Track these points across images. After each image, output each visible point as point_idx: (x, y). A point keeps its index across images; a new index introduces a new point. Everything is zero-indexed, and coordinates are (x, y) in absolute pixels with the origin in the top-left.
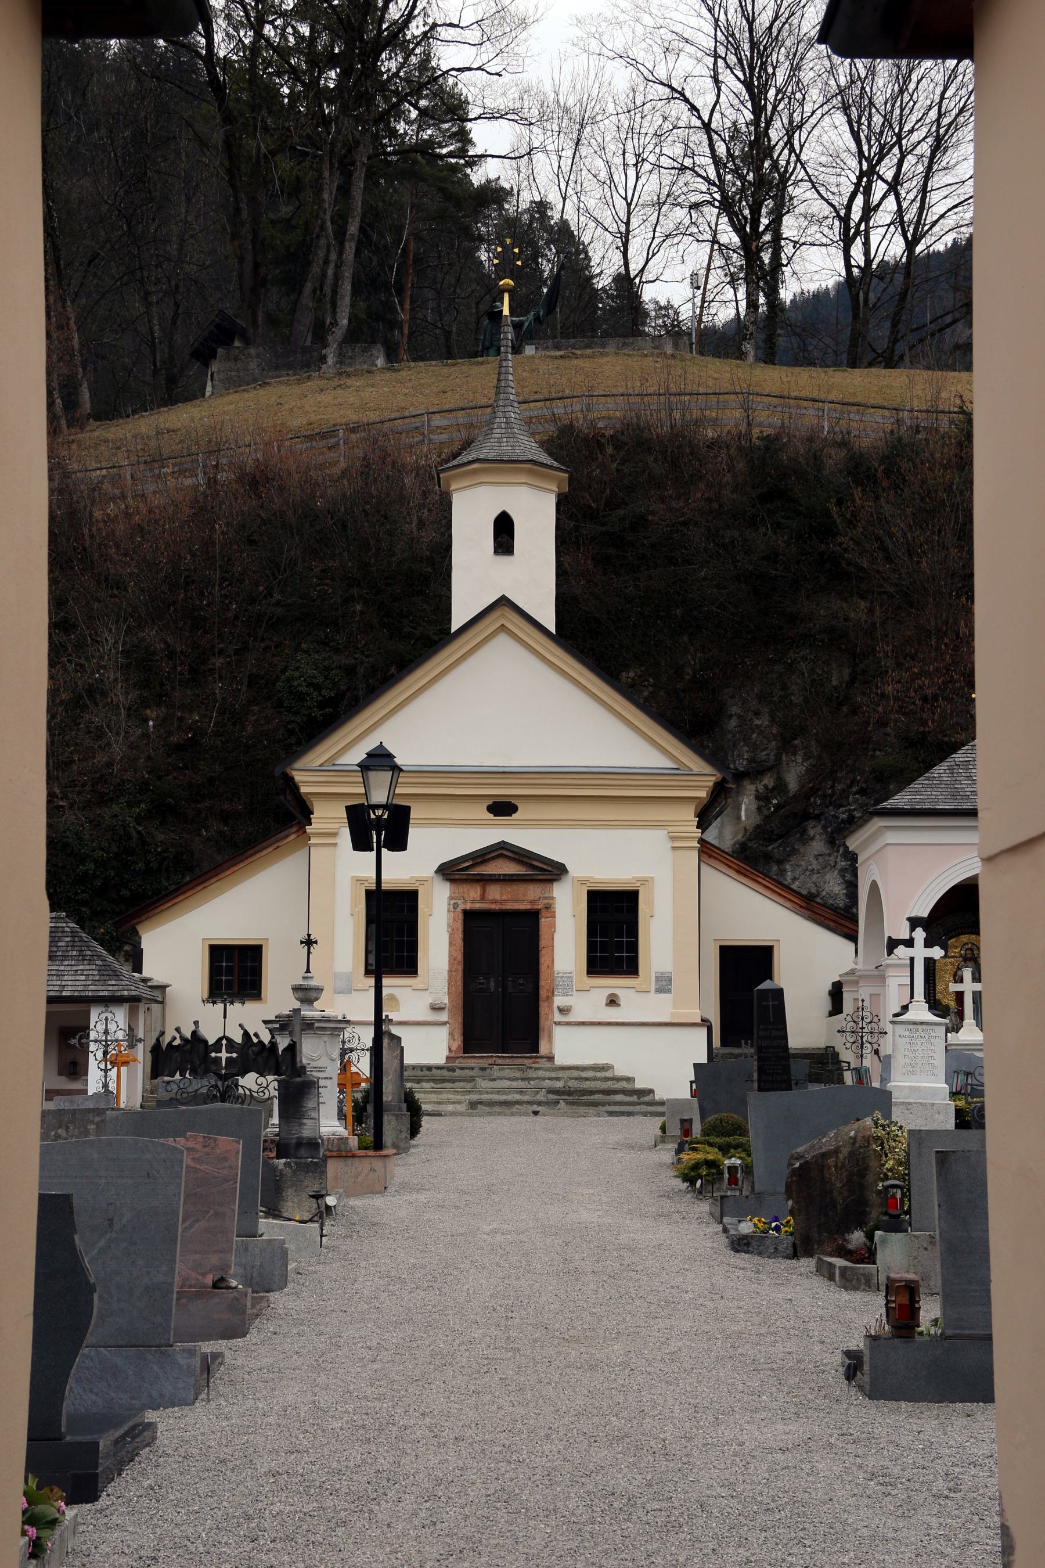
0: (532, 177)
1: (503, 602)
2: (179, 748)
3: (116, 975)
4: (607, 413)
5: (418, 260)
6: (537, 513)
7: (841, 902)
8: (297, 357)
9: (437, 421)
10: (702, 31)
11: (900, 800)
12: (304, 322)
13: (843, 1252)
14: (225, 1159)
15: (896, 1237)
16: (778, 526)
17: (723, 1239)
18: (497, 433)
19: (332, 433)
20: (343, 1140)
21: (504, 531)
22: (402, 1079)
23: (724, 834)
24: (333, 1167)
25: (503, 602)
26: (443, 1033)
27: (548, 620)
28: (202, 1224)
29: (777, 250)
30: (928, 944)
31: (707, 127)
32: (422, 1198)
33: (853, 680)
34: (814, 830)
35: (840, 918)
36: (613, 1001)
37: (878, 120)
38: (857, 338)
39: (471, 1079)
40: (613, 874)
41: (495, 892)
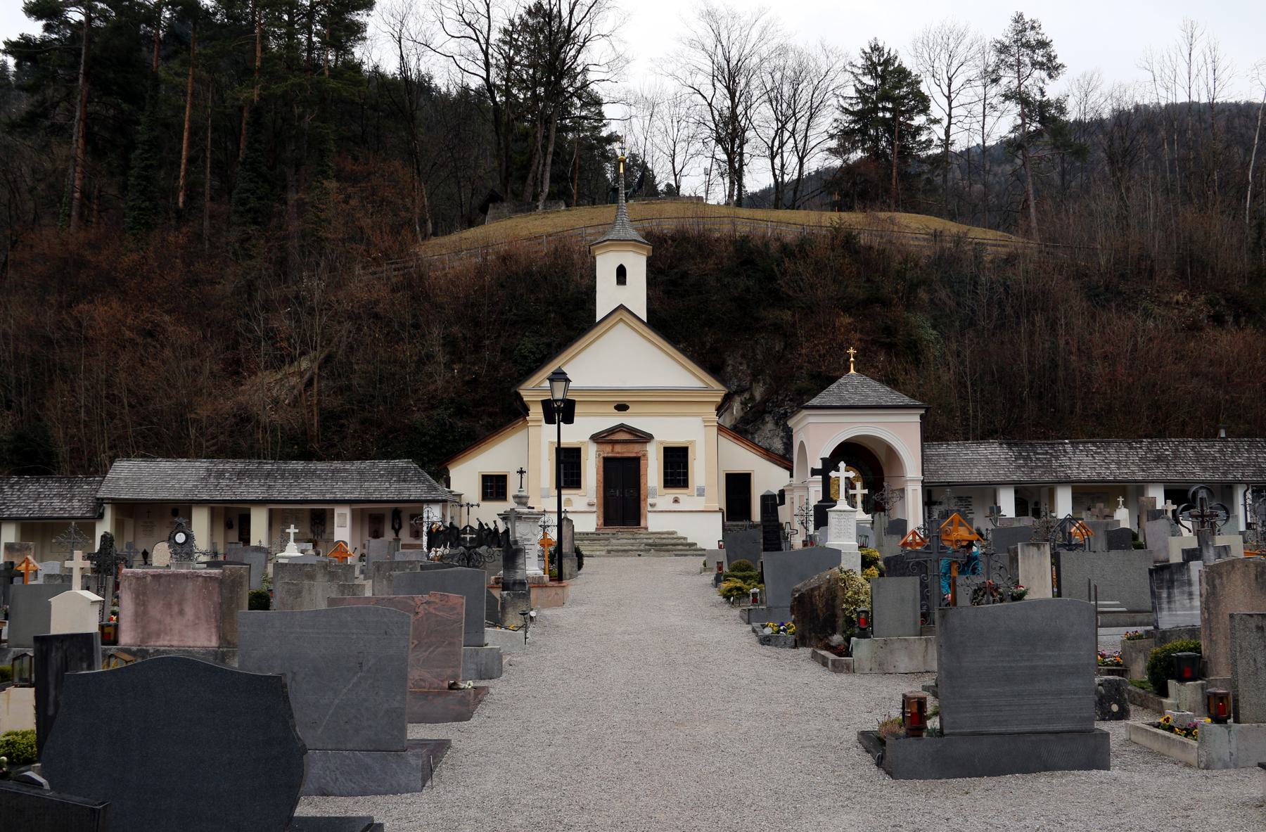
0: (631, 130)
1: (621, 307)
2: (468, 383)
3: (436, 489)
4: (668, 227)
5: (580, 167)
6: (637, 266)
7: (781, 452)
8: (526, 205)
9: (589, 231)
10: (708, 66)
11: (815, 401)
12: (529, 190)
13: (829, 648)
14: (455, 609)
15: (864, 641)
16: (748, 276)
17: (754, 639)
18: (618, 227)
19: (541, 236)
20: (541, 578)
21: (621, 273)
22: (573, 539)
23: (728, 421)
24: (534, 594)
25: (621, 307)
26: (595, 516)
27: (643, 316)
28: (440, 649)
29: (741, 160)
30: (838, 470)
31: (710, 105)
32: (583, 609)
33: (785, 348)
34: (768, 418)
35: (784, 460)
36: (676, 501)
37: (785, 106)
38: (777, 199)
39: (608, 539)
40: (676, 440)
41: (618, 448)
